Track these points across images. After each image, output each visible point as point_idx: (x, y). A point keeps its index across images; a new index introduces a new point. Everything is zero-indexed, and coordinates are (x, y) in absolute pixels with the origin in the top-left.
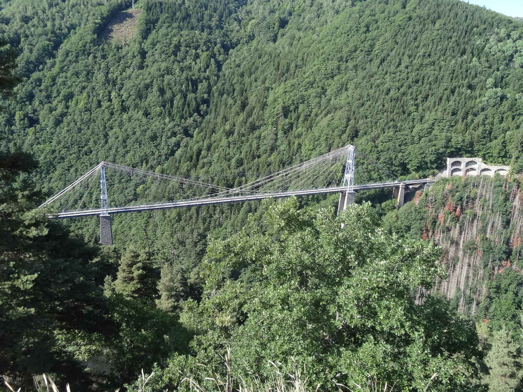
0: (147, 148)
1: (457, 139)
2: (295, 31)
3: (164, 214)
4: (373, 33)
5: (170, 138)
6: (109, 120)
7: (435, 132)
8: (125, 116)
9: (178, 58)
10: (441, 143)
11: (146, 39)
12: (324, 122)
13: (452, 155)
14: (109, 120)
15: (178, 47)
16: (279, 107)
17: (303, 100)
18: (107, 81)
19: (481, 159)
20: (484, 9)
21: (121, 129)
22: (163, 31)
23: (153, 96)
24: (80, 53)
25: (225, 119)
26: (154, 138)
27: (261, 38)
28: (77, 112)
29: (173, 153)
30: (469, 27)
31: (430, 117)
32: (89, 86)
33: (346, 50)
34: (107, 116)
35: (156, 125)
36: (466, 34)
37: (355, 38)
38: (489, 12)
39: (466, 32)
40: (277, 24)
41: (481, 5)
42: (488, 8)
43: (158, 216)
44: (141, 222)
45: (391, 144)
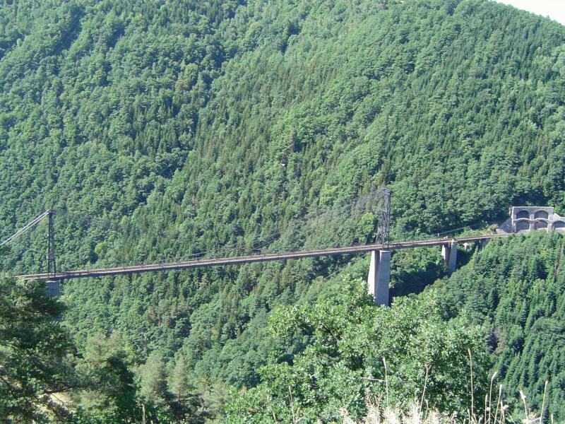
0: (106, 192)
1: (523, 185)
2: (310, 38)
3: (130, 277)
4: (413, 44)
5: (139, 177)
6: (59, 153)
7: (494, 173)
8: (80, 148)
9: (154, 72)
10: (501, 186)
11: (113, 47)
12: (347, 159)
13: (516, 202)
14: (59, 153)
15: (154, 54)
16: (288, 137)
17: (322, 130)
18: (59, 103)
19: (241, 6)
20: (548, 19)
21: (75, 165)
22: (136, 36)
23: (116, 123)
24: (26, 67)
25: (216, 154)
26: (118, 177)
27: (264, 44)
28: (18, 144)
29: (142, 199)
30: (531, 47)
31: (487, 154)
32: (35, 110)
33: (378, 64)
34: (56, 146)
35: (123, 160)
36: (527, 55)
37: (389, 48)
38: (554, 24)
39: (528, 53)
40: (286, 28)
41: (545, 16)
42: (552, 19)
43: (123, 283)
44: (278, 264)
45: (438, 188)
